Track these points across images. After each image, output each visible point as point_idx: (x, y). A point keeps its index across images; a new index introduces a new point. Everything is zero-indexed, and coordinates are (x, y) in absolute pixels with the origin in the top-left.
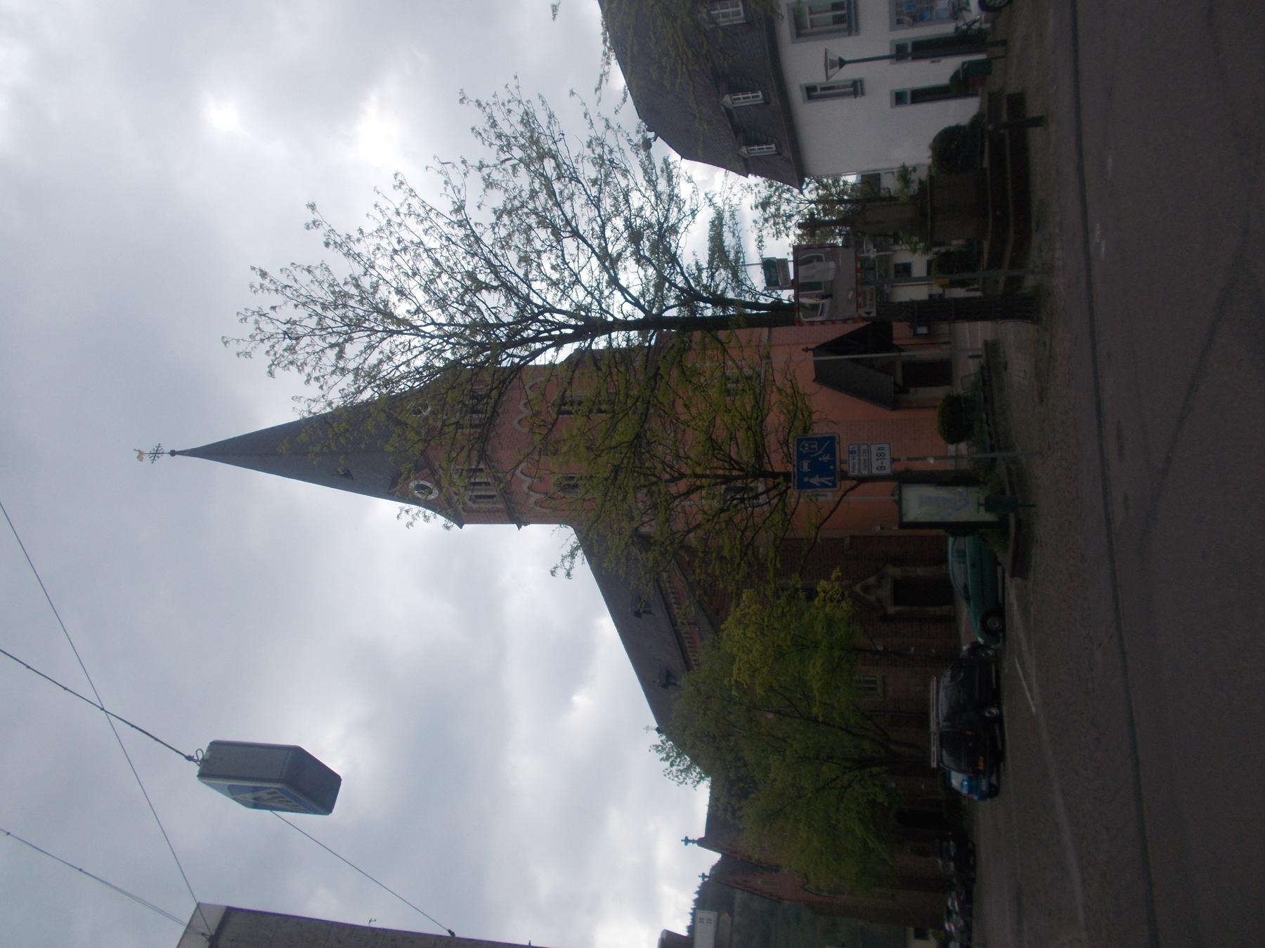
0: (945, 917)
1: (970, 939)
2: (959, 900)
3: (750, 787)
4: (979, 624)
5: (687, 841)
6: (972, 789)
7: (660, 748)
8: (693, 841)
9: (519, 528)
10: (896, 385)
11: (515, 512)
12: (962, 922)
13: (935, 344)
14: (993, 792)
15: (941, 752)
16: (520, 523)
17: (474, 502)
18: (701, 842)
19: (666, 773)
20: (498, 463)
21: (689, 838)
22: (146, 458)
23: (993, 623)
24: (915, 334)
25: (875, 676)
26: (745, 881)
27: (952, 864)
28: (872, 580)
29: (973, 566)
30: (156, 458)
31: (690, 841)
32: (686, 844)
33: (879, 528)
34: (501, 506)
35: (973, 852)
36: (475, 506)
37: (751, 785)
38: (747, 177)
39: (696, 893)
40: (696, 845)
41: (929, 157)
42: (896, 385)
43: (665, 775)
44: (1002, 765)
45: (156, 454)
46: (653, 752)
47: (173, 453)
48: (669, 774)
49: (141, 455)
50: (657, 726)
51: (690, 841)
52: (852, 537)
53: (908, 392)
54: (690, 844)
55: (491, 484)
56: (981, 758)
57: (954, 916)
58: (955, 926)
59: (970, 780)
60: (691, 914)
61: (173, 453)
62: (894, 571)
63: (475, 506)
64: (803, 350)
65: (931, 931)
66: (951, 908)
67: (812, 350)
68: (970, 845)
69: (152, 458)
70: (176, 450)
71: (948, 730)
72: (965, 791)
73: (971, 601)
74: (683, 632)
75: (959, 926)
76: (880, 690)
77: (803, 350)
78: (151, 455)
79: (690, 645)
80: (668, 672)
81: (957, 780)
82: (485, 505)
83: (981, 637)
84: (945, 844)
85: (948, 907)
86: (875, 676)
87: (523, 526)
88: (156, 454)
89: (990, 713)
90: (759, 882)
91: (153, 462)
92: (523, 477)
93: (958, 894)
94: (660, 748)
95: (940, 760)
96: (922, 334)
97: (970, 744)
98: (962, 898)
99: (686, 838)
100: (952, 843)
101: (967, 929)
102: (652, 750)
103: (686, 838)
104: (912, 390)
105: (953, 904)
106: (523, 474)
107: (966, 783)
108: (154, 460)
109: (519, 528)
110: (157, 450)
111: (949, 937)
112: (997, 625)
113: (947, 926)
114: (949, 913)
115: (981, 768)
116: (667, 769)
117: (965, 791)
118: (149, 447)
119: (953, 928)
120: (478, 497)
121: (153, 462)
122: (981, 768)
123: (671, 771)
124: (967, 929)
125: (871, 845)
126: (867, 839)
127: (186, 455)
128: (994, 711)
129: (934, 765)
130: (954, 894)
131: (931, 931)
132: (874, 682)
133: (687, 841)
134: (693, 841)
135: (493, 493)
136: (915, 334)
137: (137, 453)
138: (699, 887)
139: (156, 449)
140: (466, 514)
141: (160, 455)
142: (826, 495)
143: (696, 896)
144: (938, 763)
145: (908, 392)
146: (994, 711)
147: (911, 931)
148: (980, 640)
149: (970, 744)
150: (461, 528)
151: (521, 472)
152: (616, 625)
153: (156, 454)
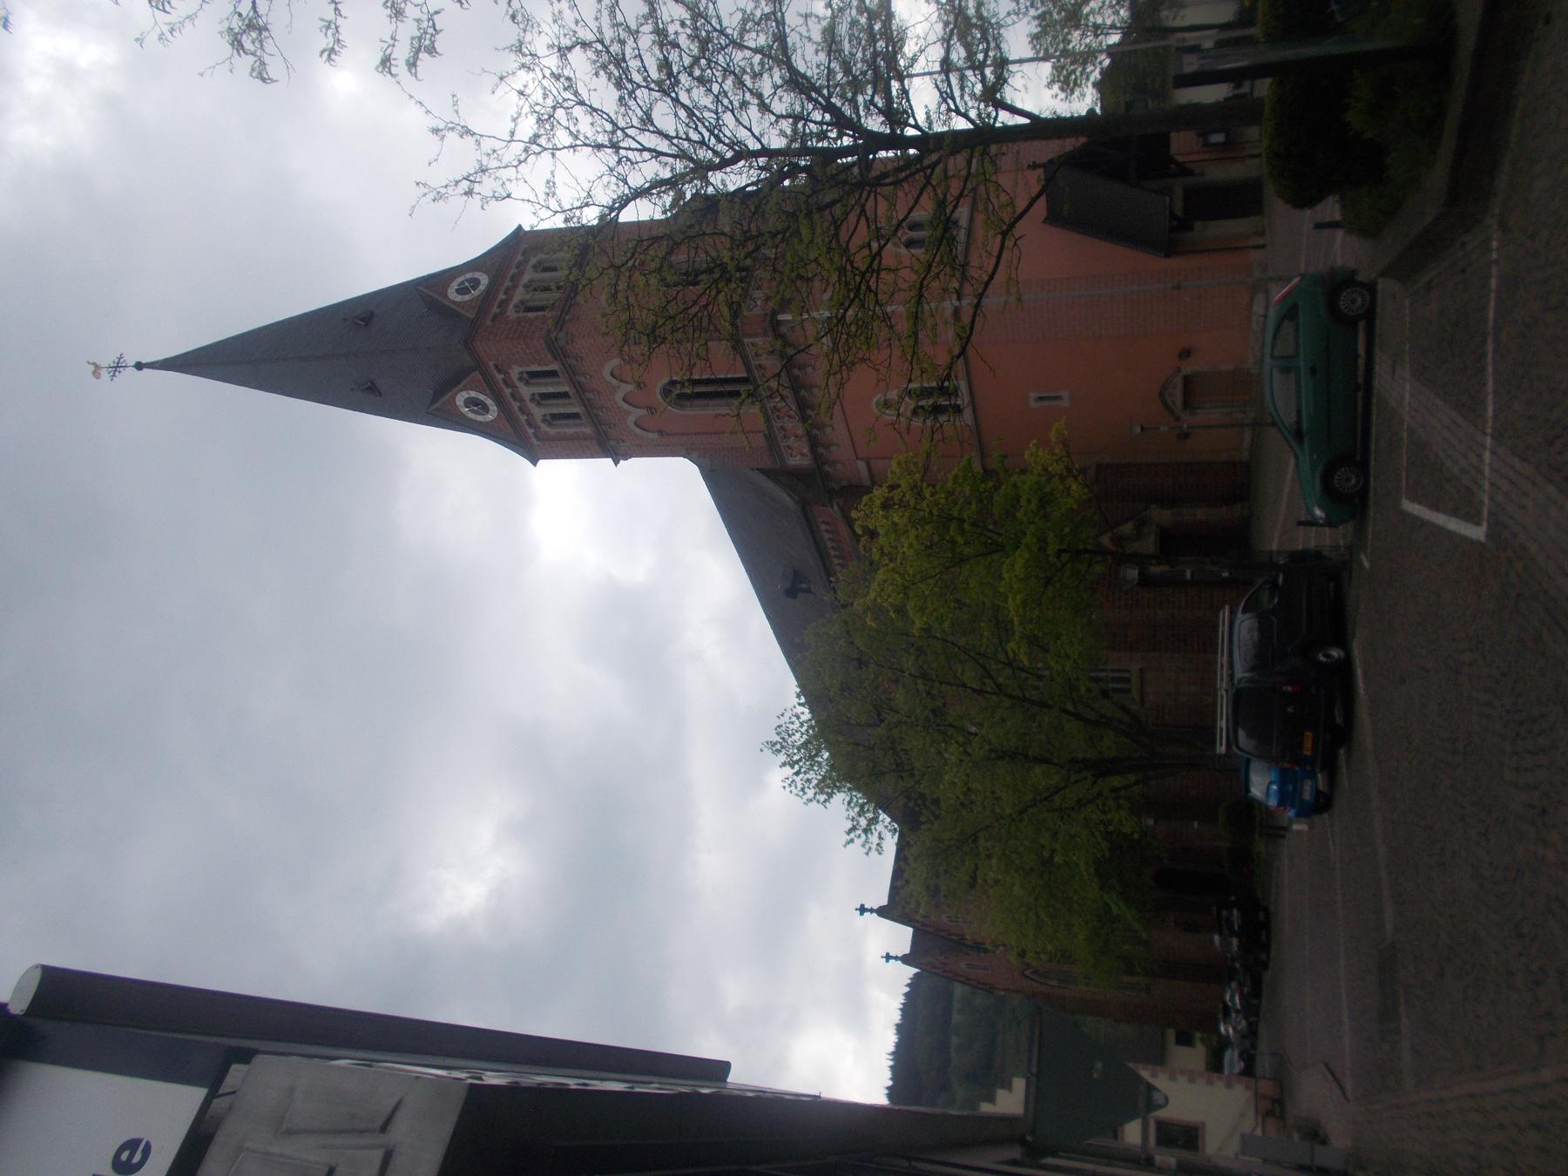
0: (1221, 1016)
1: (1254, 1046)
3: (916, 805)
4: (1318, 476)
6: (1283, 797)
7: (778, 747)
8: (871, 911)
9: (616, 463)
10: (1173, 216)
11: (608, 439)
12: (1244, 1023)
14: (1322, 804)
15: (1236, 732)
16: (617, 455)
17: (550, 425)
18: (882, 912)
19: (786, 785)
20: (577, 360)
21: (866, 907)
22: (105, 374)
23: (1346, 480)
24: (1206, 145)
27: (1235, 941)
28: (1128, 528)
29: (1313, 371)
30: (117, 373)
31: (867, 910)
33: (1139, 430)
34: (588, 430)
37: (919, 802)
39: (907, 986)
42: (1173, 216)
43: (784, 787)
44: (1342, 751)
45: (117, 367)
46: (768, 752)
47: (139, 366)
48: (790, 785)
51: (867, 910)
53: (1190, 228)
56: (1309, 734)
57: (1234, 1015)
58: (1234, 1029)
59: (1282, 783)
60: (900, 1009)
61: (139, 366)
62: (1161, 515)
63: (552, 431)
65: (1198, 1035)
66: (1230, 1004)
68: (1261, 916)
69: (112, 374)
70: (144, 361)
72: (1273, 802)
73: (1306, 440)
75: (1239, 1028)
76: (1135, 694)
78: (110, 369)
81: (1261, 785)
83: (1320, 507)
84: (1224, 913)
87: (621, 461)
88: (117, 367)
89: (1326, 656)
90: (963, 965)
91: (112, 380)
92: (626, 406)
93: (1241, 985)
94: (778, 747)
95: (1232, 741)
96: (1216, 145)
97: (1290, 710)
99: (862, 906)
100: (1235, 912)
101: (1252, 1032)
102: (765, 750)
103: (862, 906)
104: (1198, 224)
105: (1232, 998)
106: (626, 402)
108: (114, 375)
109: (616, 463)
110: (115, 371)
111: (1224, 1043)
112: (1353, 481)
113: (1222, 1029)
114: (1226, 1011)
116: (788, 779)
117: (1273, 802)
118: (107, 360)
119: (1231, 1031)
120: (555, 417)
121: (112, 380)
123: (794, 780)
124: (1252, 1032)
125: (1115, 910)
126: (1110, 902)
127: (157, 368)
128: (1335, 653)
130: (1234, 985)
131: (1198, 1035)
132: (1128, 680)
134: (871, 911)
136: (1206, 145)
137: (92, 368)
138: (911, 979)
139: (116, 361)
140: (539, 443)
141: (122, 369)
143: (908, 989)
144: (1228, 746)
146: (1335, 653)
147: (1171, 1034)
148: (1318, 512)
149: (1290, 710)
150: (535, 465)
152: (769, 618)
153: (117, 367)
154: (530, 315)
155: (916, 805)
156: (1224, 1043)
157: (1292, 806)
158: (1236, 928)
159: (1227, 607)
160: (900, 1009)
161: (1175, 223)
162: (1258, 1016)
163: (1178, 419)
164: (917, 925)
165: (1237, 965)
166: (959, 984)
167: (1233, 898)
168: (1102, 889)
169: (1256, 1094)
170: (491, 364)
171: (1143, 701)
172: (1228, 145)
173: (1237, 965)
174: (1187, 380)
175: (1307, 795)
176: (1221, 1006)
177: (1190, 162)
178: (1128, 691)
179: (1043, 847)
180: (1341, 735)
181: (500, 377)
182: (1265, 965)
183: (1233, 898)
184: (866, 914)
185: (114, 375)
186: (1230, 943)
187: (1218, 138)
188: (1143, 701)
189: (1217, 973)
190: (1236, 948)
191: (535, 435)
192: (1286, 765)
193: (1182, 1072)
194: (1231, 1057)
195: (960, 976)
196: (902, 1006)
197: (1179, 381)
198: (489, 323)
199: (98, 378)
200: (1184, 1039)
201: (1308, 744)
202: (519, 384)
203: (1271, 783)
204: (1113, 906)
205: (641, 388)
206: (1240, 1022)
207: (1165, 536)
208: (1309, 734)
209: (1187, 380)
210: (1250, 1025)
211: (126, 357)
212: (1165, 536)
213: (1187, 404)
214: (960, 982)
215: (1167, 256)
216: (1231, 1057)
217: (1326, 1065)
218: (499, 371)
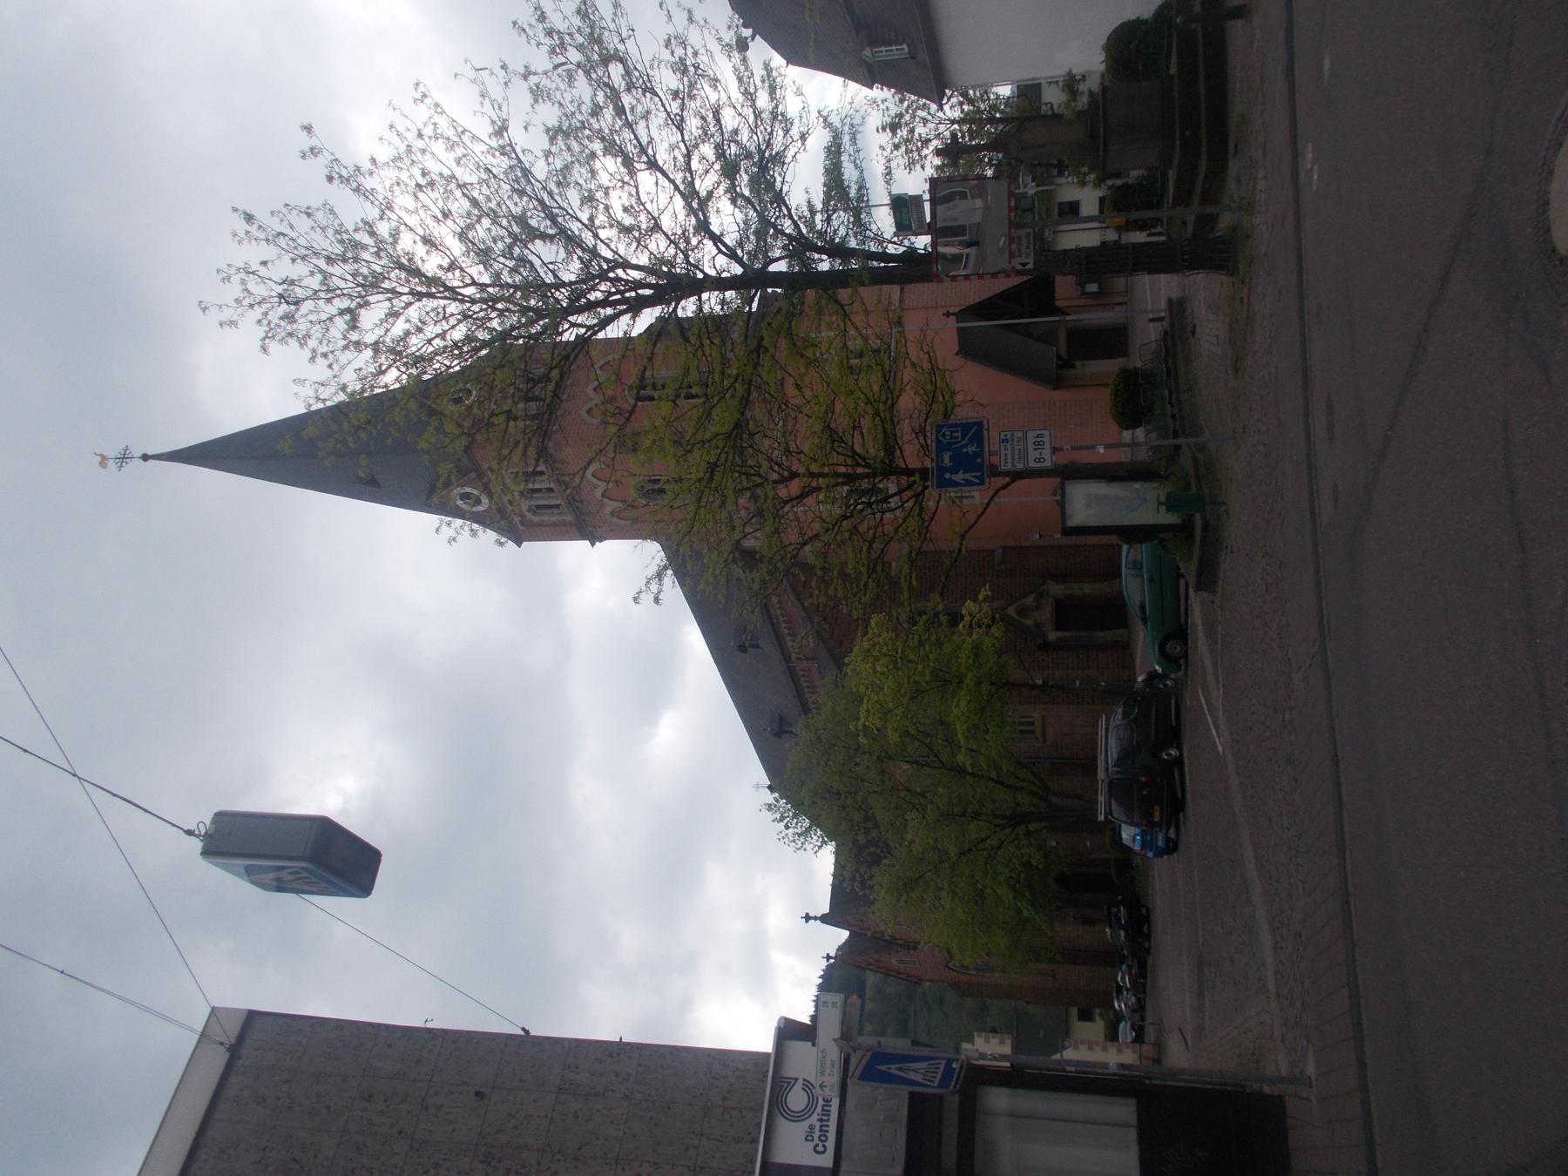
1: (1143, 1019)
2: (1130, 974)
4: (1157, 648)
5: (808, 918)
8: (815, 918)
9: (593, 545)
10: (1059, 357)
12: (1133, 999)
14: (1171, 847)
17: (534, 514)
18: (825, 919)
20: (563, 464)
22: (111, 463)
23: (1174, 648)
24: (1083, 294)
27: (1122, 933)
28: (1029, 600)
29: (1151, 579)
30: (124, 464)
31: (812, 918)
33: (1038, 537)
34: (569, 518)
35: (1147, 919)
36: (536, 519)
39: (820, 978)
42: (1059, 357)
43: (779, 839)
44: (1181, 814)
46: (765, 811)
47: (145, 457)
48: (784, 838)
49: (104, 461)
51: (812, 918)
52: (1004, 548)
53: (1073, 366)
55: (555, 490)
56: (1157, 808)
57: (1125, 993)
59: (1143, 834)
61: (145, 457)
62: (1056, 589)
63: (536, 519)
64: (944, 315)
67: (953, 314)
68: (1144, 911)
69: (119, 464)
70: (150, 453)
72: (1137, 847)
77: (944, 315)
78: (117, 460)
82: (547, 518)
84: (1114, 910)
86: (1033, 717)
87: (597, 543)
88: (124, 458)
89: (1168, 755)
90: (894, 961)
91: (120, 470)
92: (595, 481)
95: (1109, 812)
97: (1144, 792)
98: (1134, 972)
99: (807, 914)
100: (1122, 908)
101: (1140, 1008)
104: (1078, 364)
105: (1123, 978)
107: (1138, 838)
108: (121, 466)
109: (593, 545)
111: (1119, 1017)
114: (1119, 989)
117: (1137, 847)
118: (114, 451)
119: (1123, 1006)
120: (539, 507)
121: (120, 470)
124: (1140, 1008)
125: (1026, 914)
126: (1022, 908)
128: (1173, 752)
129: (1101, 818)
130: (1124, 967)
131: (1098, 1011)
132: (1032, 724)
133: (808, 918)
134: (815, 918)
135: (558, 502)
137: (99, 459)
141: (128, 460)
143: (821, 981)
144: (1106, 817)
145: (1073, 366)
147: (1074, 1011)
149: (1144, 792)
150: (519, 546)
153: (124, 458)
155: (882, 852)
156: (1119, 1017)
157: (1151, 850)
158: (1123, 922)
159: (1104, 716)
160: (814, 1001)
161: (1060, 362)
162: (1144, 992)
164: (854, 929)
165: (1125, 952)
166: (870, 972)
167: (1120, 898)
168: (1015, 898)
169: (1140, 1056)
171: (1045, 741)
172: (1101, 293)
173: (1125, 952)
175: (1161, 842)
176: (1115, 985)
177: (1068, 307)
178: (1033, 732)
179: (978, 881)
180: (1177, 808)
182: (1148, 951)
183: (1120, 898)
184: (810, 921)
185: (121, 466)
186: (1120, 935)
187: (1093, 288)
188: (1045, 741)
189: (1110, 958)
190: (1123, 938)
191: (521, 522)
192: (1145, 828)
193: (1083, 1042)
194: (1125, 1029)
195: (891, 970)
196: (815, 999)
199: (105, 468)
200: (1086, 1016)
201: (1157, 814)
203: (1137, 835)
204: (1024, 911)
205: (618, 486)
206: (1131, 998)
207: (1059, 605)
208: (1157, 808)
210: (1138, 1000)
211: (132, 449)
212: (1059, 605)
214: (872, 970)
215: (1055, 389)
216: (1125, 1029)
217: (1180, 1030)
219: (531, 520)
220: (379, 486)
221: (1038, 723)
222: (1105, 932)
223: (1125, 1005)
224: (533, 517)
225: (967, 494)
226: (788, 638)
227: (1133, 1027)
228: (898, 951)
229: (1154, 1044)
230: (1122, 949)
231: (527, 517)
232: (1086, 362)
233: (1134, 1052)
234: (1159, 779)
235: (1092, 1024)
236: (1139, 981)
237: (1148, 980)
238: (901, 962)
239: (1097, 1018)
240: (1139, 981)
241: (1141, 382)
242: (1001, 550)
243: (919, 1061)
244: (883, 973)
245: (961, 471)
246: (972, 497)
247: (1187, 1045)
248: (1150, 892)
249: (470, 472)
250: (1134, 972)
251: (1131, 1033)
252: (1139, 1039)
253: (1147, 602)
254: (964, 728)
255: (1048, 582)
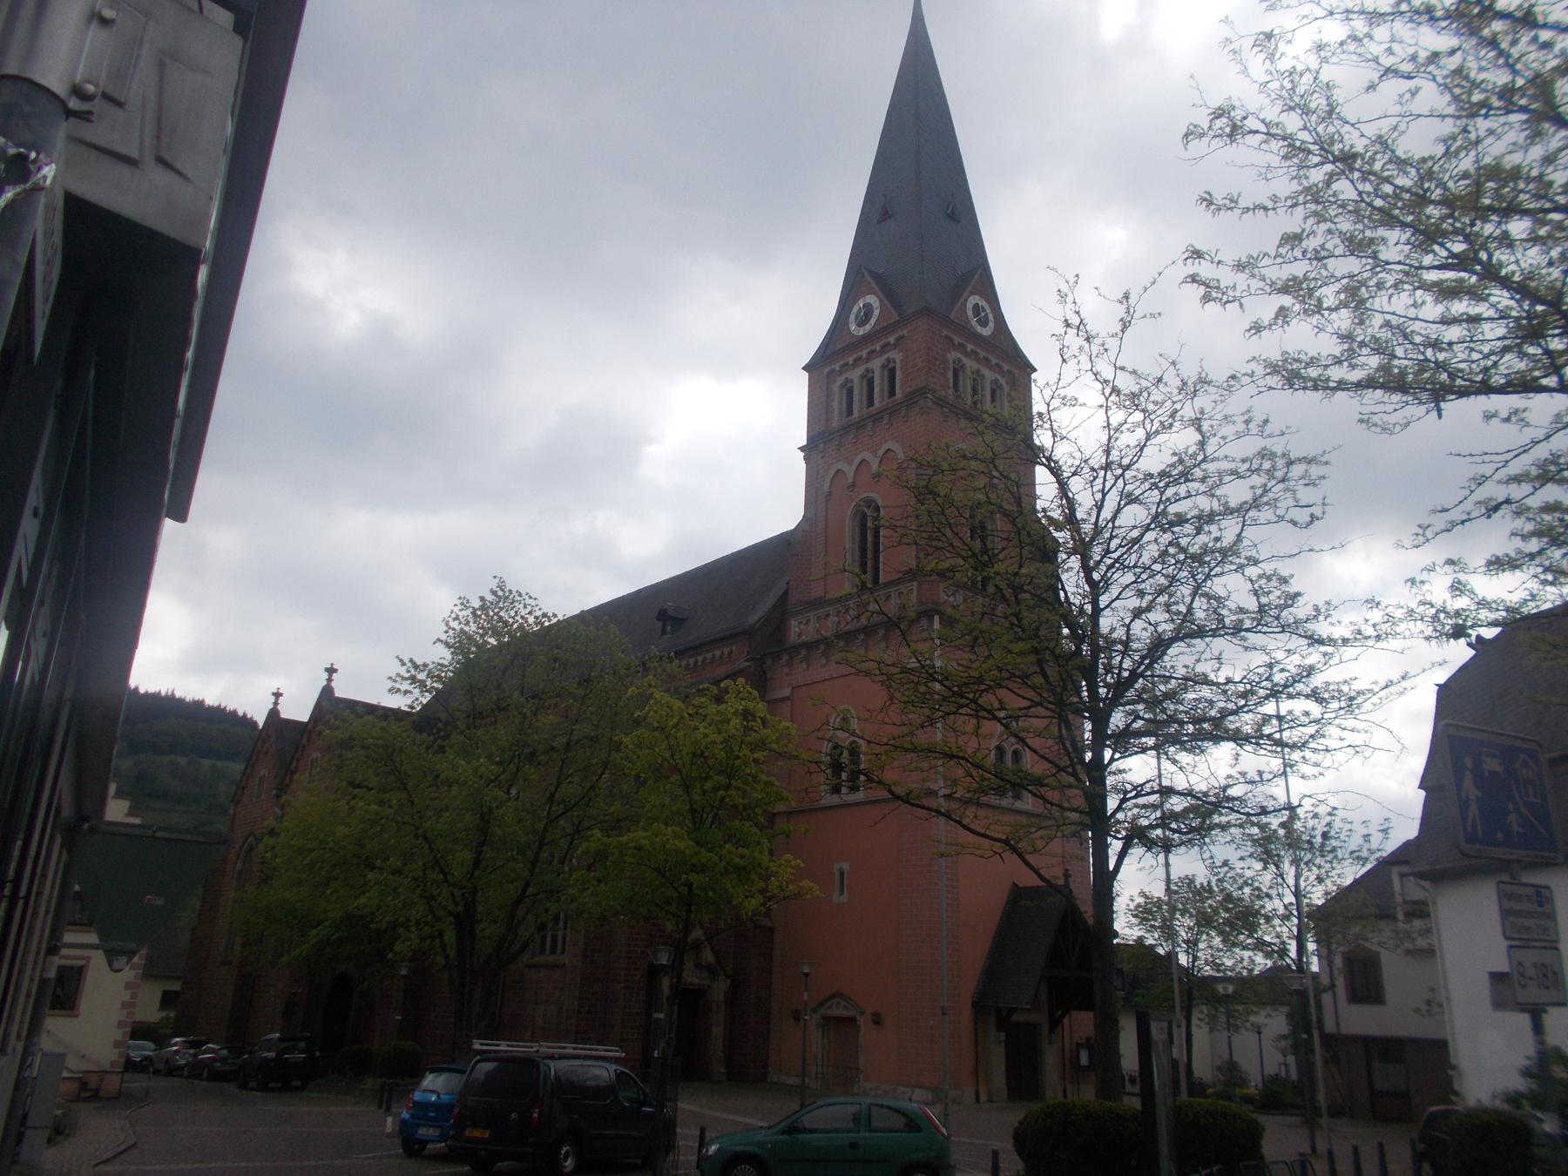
1: (156, 1072)
2: (213, 1060)
5: (331, 671)
6: (424, 1106)
8: (330, 680)
9: (802, 449)
10: (1012, 1011)
13: (1064, 1079)
14: (412, 1147)
17: (842, 386)
18: (327, 691)
25: (563, 952)
26: (267, 752)
27: (272, 1054)
28: (708, 956)
29: (854, 1146)
31: (330, 675)
32: (274, 694)
34: (835, 423)
35: (286, 1088)
38: (1420, 787)
40: (271, 706)
41: (1479, 1101)
42: (1012, 1011)
50: (337, 695)
51: (330, 675)
52: (772, 930)
53: (999, 1030)
54: (326, 675)
55: (871, 409)
57: (192, 1051)
59: (437, 1106)
62: (719, 990)
63: (836, 388)
65: (172, 1014)
68: (296, 1083)
71: (542, 1073)
72: (417, 1096)
73: (786, 1137)
74: (734, 648)
76: (539, 959)
79: (717, 658)
80: (683, 620)
81: (435, 1086)
82: (837, 406)
84: (302, 1044)
85: (205, 1043)
86: (563, 952)
90: (264, 772)
92: (856, 462)
93: (224, 1060)
95: (485, 1056)
97: (514, 1115)
99: (281, 695)
101: (172, 1070)
103: (281, 695)
104: (1002, 1036)
107: (433, 1098)
111: (161, 1041)
114: (196, 1045)
115: (467, 1133)
117: (417, 1096)
119: (175, 1048)
122: (467, 1133)
124: (172, 1070)
125: (313, 933)
127: (914, 8)
129: (477, 1045)
130: (225, 1052)
131: (172, 1014)
132: (553, 951)
133: (331, 671)
134: (330, 680)
135: (877, 403)
140: (825, 373)
142: (842, 892)
143: (241, 714)
144: (479, 1052)
145: (999, 1030)
147: (176, 986)
148: (713, 1148)
150: (804, 368)
151: (864, 460)
154: (950, 375)
156: (161, 1041)
157: (413, 1116)
161: (1005, 1013)
162: (189, 1077)
163: (814, 1010)
169: (105, 1072)
170: (905, 332)
174: (853, 1020)
179: (386, 859)
181: (891, 340)
182: (244, 1086)
183: (318, 1054)
187: (1084, 1059)
193: (134, 996)
194: (147, 1048)
197: (852, 1013)
198: (945, 333)
200: (168, 1000)
201: (477, 1133)
202: (882, 359)
203: (439, 1097)
209: (853, 1020)
210: (181, 1068)
213: (828, 1020)
215: (974, 1005)
216: (147, 1048)
217: (134, 1145)
218: (897, 340)
219: (835, 382)
220: (880, 222)
221: (551, 959)
222: (272, 1031)
223: (176, 1051)
224: (838, 384)
225: (569, 925)
226: (692, 661)
227: (147, 1058)
228: (275, 777)
229: (120, 1091)
230: (250, 1053)
231: (838, 378)
232: (1003, 1045)
233: (113, 1064)
234: (532, 1140)
235: (157, 1006)
236: (206, 1070)
237: (205, 1083)
238: (262, 779)
239: (164, 1014)
240: (206, 1070)
241: (1241, 1165)
242: (769, 924)
243: (34, 261)
244: (241, 780)
245: (1480, 795)
246: (842, 892)
247: (105, 1162)
248: (325, 1096)
249: (899, 314)
250: (218, 1064)
251: (141, 1056)
252: (130, 1066)
253: (743, 1120)
254: (643, 842)
255: (728, 981)
